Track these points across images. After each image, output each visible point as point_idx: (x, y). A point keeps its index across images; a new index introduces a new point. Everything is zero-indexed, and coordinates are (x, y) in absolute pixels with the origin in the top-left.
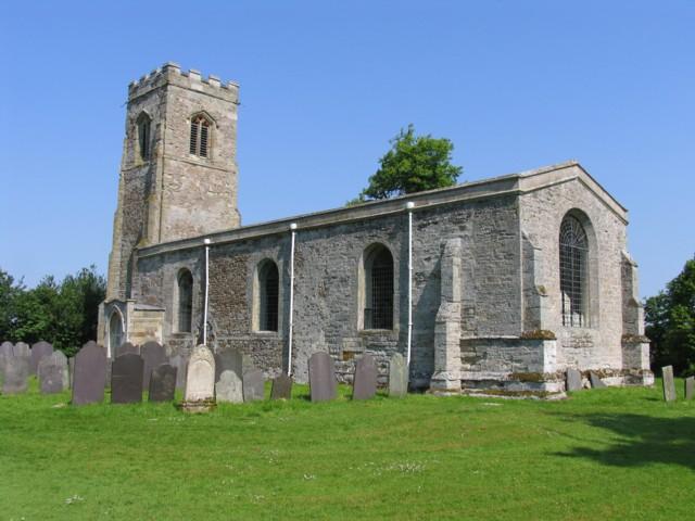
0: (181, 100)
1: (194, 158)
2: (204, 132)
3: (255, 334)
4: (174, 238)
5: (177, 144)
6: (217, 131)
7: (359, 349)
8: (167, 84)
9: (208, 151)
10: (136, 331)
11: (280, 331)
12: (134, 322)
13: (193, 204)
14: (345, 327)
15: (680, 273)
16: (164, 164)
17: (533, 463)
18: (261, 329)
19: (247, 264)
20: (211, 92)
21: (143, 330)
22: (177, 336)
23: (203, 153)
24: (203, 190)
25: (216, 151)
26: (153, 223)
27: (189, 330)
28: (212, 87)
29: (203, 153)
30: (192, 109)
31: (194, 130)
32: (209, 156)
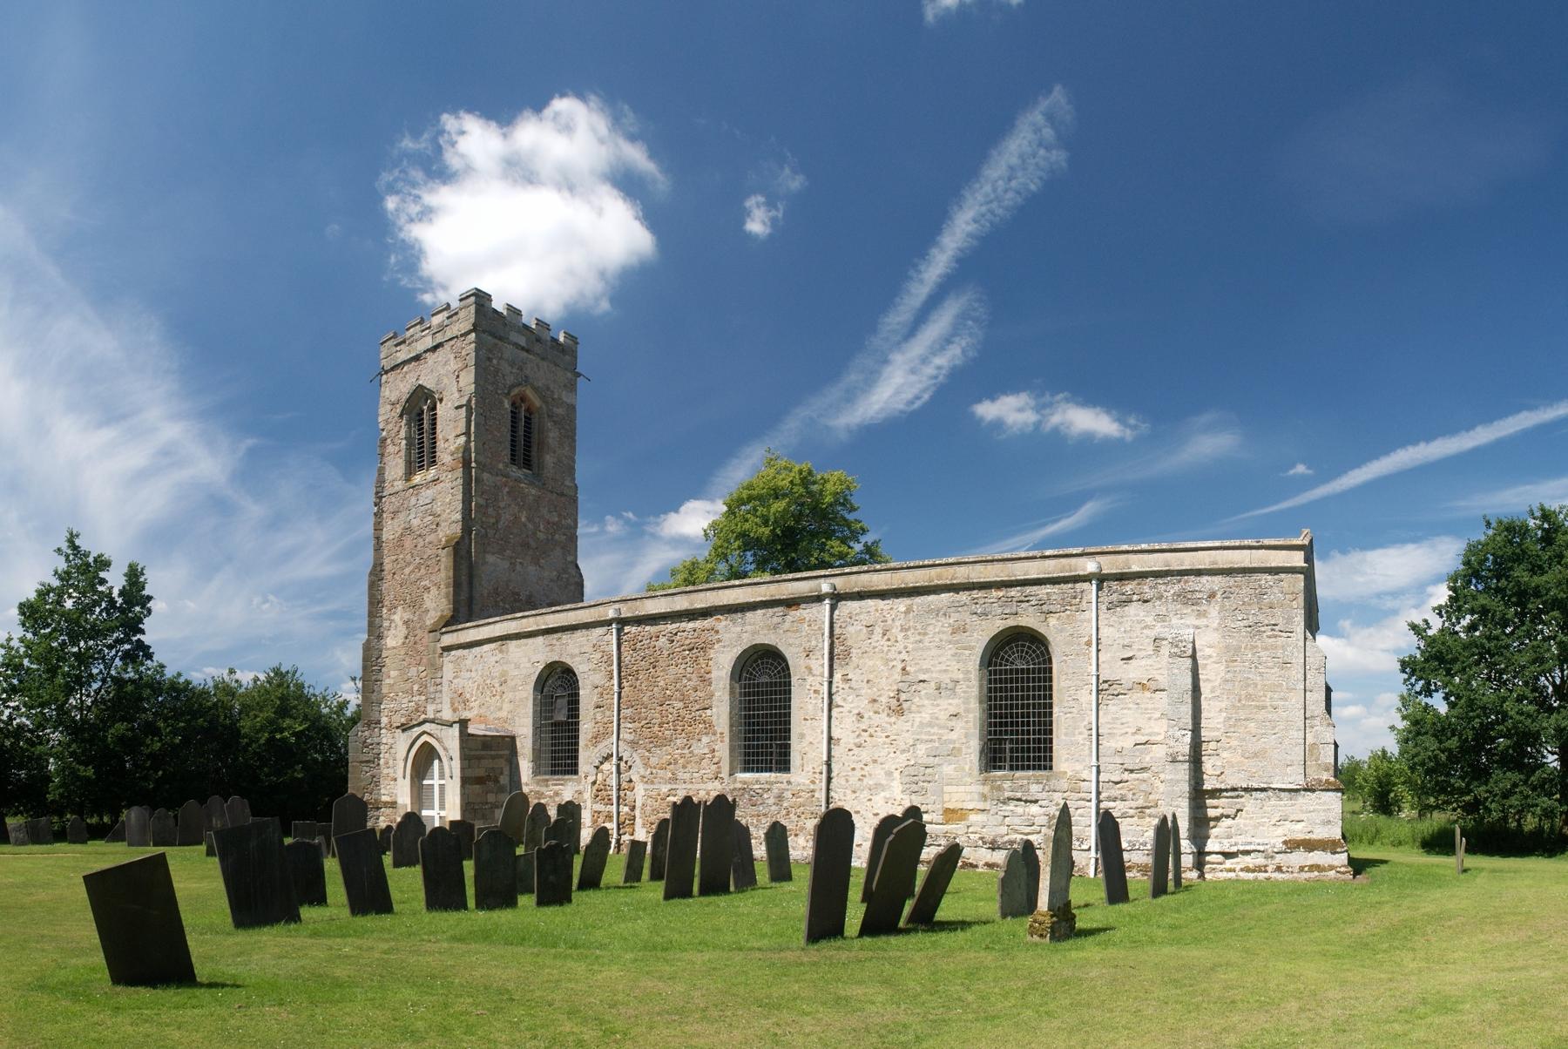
7: (981, 806)
9: (534, 460)
23: (527, 464)
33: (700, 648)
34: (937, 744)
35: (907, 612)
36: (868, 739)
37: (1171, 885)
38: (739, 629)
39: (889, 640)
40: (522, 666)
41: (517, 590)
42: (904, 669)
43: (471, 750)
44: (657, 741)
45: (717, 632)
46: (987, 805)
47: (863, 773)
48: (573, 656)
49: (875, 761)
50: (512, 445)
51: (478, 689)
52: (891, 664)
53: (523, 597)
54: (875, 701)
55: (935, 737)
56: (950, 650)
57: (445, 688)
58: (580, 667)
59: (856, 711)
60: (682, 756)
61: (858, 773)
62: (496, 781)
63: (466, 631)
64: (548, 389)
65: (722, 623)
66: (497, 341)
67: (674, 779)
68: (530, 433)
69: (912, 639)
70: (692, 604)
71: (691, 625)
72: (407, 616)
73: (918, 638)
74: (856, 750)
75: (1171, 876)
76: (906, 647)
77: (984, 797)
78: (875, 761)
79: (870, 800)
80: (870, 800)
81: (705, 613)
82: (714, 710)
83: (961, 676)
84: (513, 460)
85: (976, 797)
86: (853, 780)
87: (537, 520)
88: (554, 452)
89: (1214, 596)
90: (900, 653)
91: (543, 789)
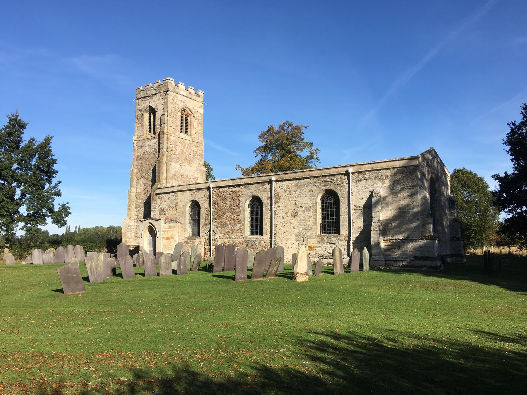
0: (175, 101)
1: (182, 135)
2: (187, 119)
3: (247, 237)
4: (175, 183)
5: (174, 127)
6: (194, 119)
7: (318, 245)
8: (168, 91)
9: (189, 131)
10: (166, 236)
11: (266, 236)
12: (164, 231)
13: (183, 162)
14: (309, 234)
15: (89, 227)
16: (167, 138)
17: (72, 375)
18: (252, 234)
19: (240, 199)
20: (189, 96)
21: (169, 236)
22: (189, 238)
23: (186, 132)
24: (187, 154)
25: (194, 131)
26: (163, 173)
27: (199, 235)
28: (190, 93)
29: (186, 132)
30: (181, 106)
31: (182, 117)
32: (189, 134)
33: (236, 197)
34: (305, 226)
35: (296, 185)
36: (285, 225)
37: (332, 271)
38: (248, 191)
39: (291, 194)
40: (183, 201)
41: (182, 174)
42: (295, 203)
43: (165, 228)
44: (225, 226)
45: (241, 192)
46: (320, 245)
47: (284, 235)
48: (199, 198)
49: (287, 232)
50: (181, 127)
51: (168, 208)
52: (291, 202)
53: (185, 176)
54: (287, 213)
55: (305, 224)
56: (308, 197)
57: (157, 207)
58: (201, 202)
59: (281, 216)
60: (232, 230)
61: (283, 235)
62: (173, 238)
63: (164, 189)
64: (194, 108)
65: (242, 189)
66: (176, 94)
67: (229, 238)
68: (187, 123)
69: (297, 194)
70: (234, 183)
71: (235, 190)
72: (145, 182)
73: (299, 193)
74: (282, 228)
75: (289, 275)
76: (295, 196)
77: (319, 242)
78: (287, 232)
79: (286, 243)
80: (286, 243)
81: (238, 186)
82: (241, 216)
83: (312, 205)
84: (181, 132)
85: (317, 242)
86: (282, 236)
87: (190, 151)
88: (196, 129)
89: (388, 177)
90: (294, 198)
91: (189, 241)
